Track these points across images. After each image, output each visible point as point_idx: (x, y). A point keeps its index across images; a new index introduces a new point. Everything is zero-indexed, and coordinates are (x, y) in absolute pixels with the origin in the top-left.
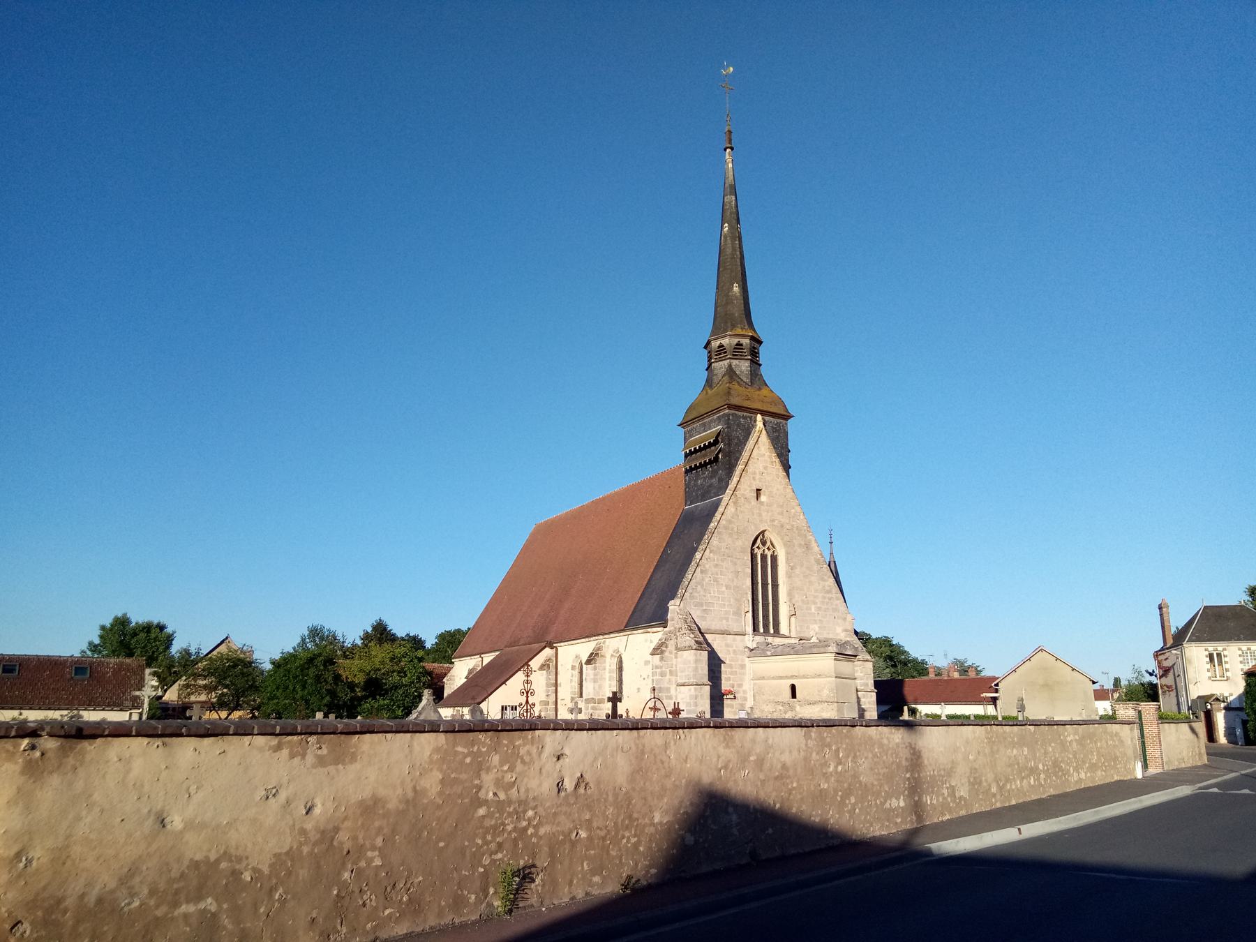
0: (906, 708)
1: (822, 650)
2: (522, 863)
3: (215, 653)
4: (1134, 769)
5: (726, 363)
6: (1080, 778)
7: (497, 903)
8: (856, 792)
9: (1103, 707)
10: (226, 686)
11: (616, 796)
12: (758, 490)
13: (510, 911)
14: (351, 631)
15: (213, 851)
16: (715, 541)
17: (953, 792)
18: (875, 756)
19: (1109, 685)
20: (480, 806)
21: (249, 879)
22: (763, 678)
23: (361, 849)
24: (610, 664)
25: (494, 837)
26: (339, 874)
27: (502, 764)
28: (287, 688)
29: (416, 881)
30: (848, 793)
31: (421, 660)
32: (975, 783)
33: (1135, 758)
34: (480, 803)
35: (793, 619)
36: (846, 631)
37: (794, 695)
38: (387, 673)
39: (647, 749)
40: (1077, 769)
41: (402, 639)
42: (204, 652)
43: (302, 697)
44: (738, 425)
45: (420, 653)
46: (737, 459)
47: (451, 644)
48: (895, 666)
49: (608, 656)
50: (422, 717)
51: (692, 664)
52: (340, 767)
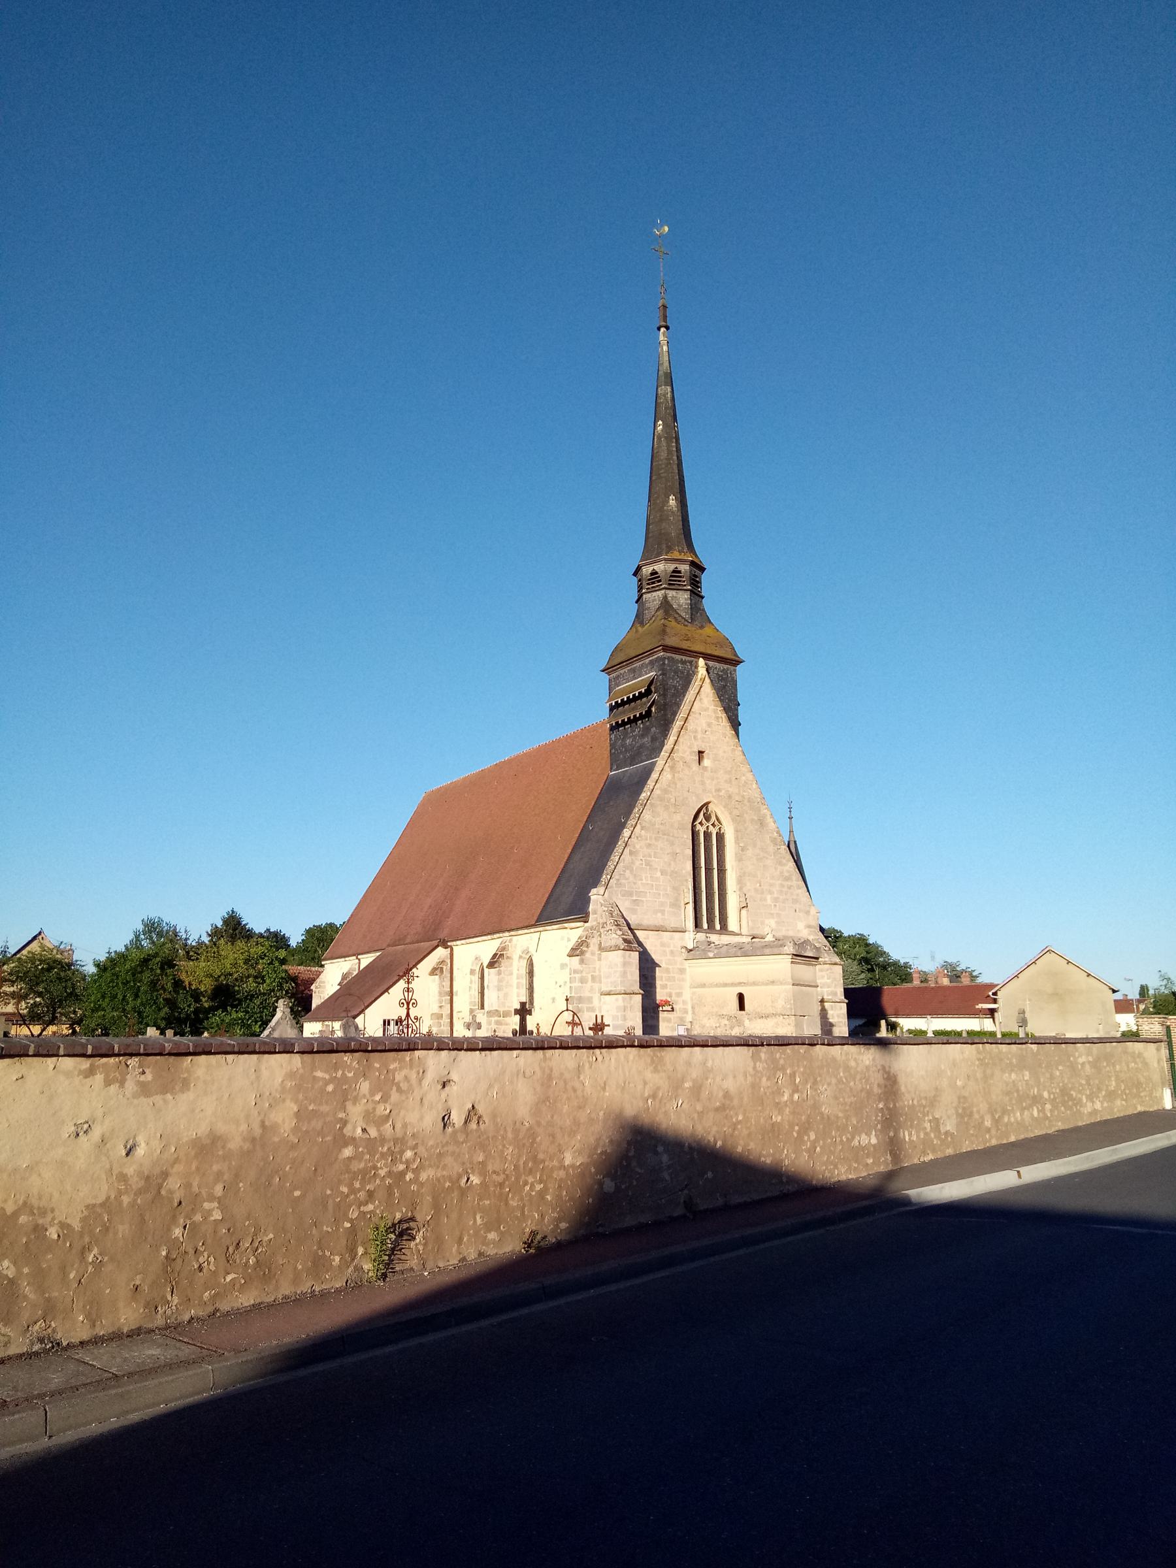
0: (883, 1022)
1: (776, 951)
2: (398, 1216)
3: (24, 952)
4: (1162, 1098)
5: (660, 593)
6: (1095, 1108)
7: (367, 1266)
8: (818, 1124)
9: (1127, 1021)
10: (40, 995)
11: (516, 1132)
12: (701, 753)
13: (384, 1276)
14: (196, 926)
15: (10, 1202)
16: (647, 815)
17: (938, 1125)
18: (840, 1081)
19: (1134, 995)
20: (346, 1145)
21: (56, 1237)
22: (703, 986)
23: (196, 1200)
24: (517, 967)
25: (364, 1182)
26: (169, 1230)
27: (372, 1094)
28: (115, 996)
29: (266, 1239)
30: (805, 1129)
31: (283, 962)
32: (965, 1114)
33: (1163, 1085)
34: (343, 1141)
35: (744, 911)
36: (809, 927)
37: (742, 1007)
38: (241, 979)
39: (556, 1073)
40: (1090, 1098)
41: (261, 936)
42: (12, 950)
43: (134, 1009)
44: (676, 672)
45: (282, 954)
46: (675, 714)
47: (321, 942)
48: (871, 970)
49: (515, 957)
50: (276, 1035)
51: (620, 968)
52: (169, 1096)
